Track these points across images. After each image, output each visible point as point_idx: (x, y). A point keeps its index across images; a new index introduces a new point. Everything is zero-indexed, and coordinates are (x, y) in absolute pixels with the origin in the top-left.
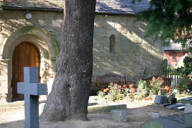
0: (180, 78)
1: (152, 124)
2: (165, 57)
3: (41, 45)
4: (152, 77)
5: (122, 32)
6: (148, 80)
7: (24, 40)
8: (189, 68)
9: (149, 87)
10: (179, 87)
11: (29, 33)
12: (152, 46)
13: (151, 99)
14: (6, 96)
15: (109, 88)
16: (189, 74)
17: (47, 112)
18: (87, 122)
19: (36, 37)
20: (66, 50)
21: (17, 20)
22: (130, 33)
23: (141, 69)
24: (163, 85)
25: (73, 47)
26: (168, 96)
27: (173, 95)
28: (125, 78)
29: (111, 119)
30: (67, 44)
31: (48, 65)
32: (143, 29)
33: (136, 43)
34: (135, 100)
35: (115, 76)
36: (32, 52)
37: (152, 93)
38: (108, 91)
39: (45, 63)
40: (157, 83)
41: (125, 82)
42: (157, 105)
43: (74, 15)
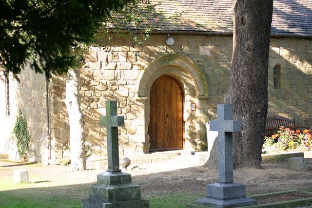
3: (186, 78)
5: (290, 60)
7: (164, 73)
11: (171, 63)
14: (142, 145)
15: (279, 134)
17: (214, 159)
18: (260, 170)
19: (179, 68)
21: (156, 47)
22: (301, 61)
25: (245, 82)
28: (294, 122)
29: (289, 168)
30: (237, 79)
31: (194, 105)
33: (309, 75)
35: (281, 119)
36: (174, 88)
39: (190, 103)
43: (246, 45)
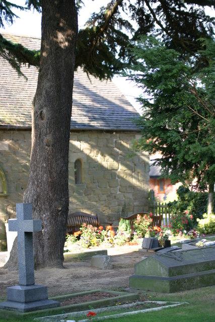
0: (172, 216)
1: (147, 263)
2: (148, 188)
4: (136, 215)
6: (132, 219)
8: (186, 202)
9: (133, 229)
10: (173, 228)
12: (133, 172)
13: (136, 244)
16: (185, 210)
20: (36, 183)
22: (103, 155)
23: (119, 205)
24: (151, 225)
26: (159, 238)
27: (166, 237)
28: (97, 219)
29: (92, 266)
32: (119, 149)
33: (110, 169)
34: (116, 246)
37: (137, 237)
38: (80, 235)
40: (144, 222)
41: (101, 223)
42: (145, 250)
43: (45, 141)
